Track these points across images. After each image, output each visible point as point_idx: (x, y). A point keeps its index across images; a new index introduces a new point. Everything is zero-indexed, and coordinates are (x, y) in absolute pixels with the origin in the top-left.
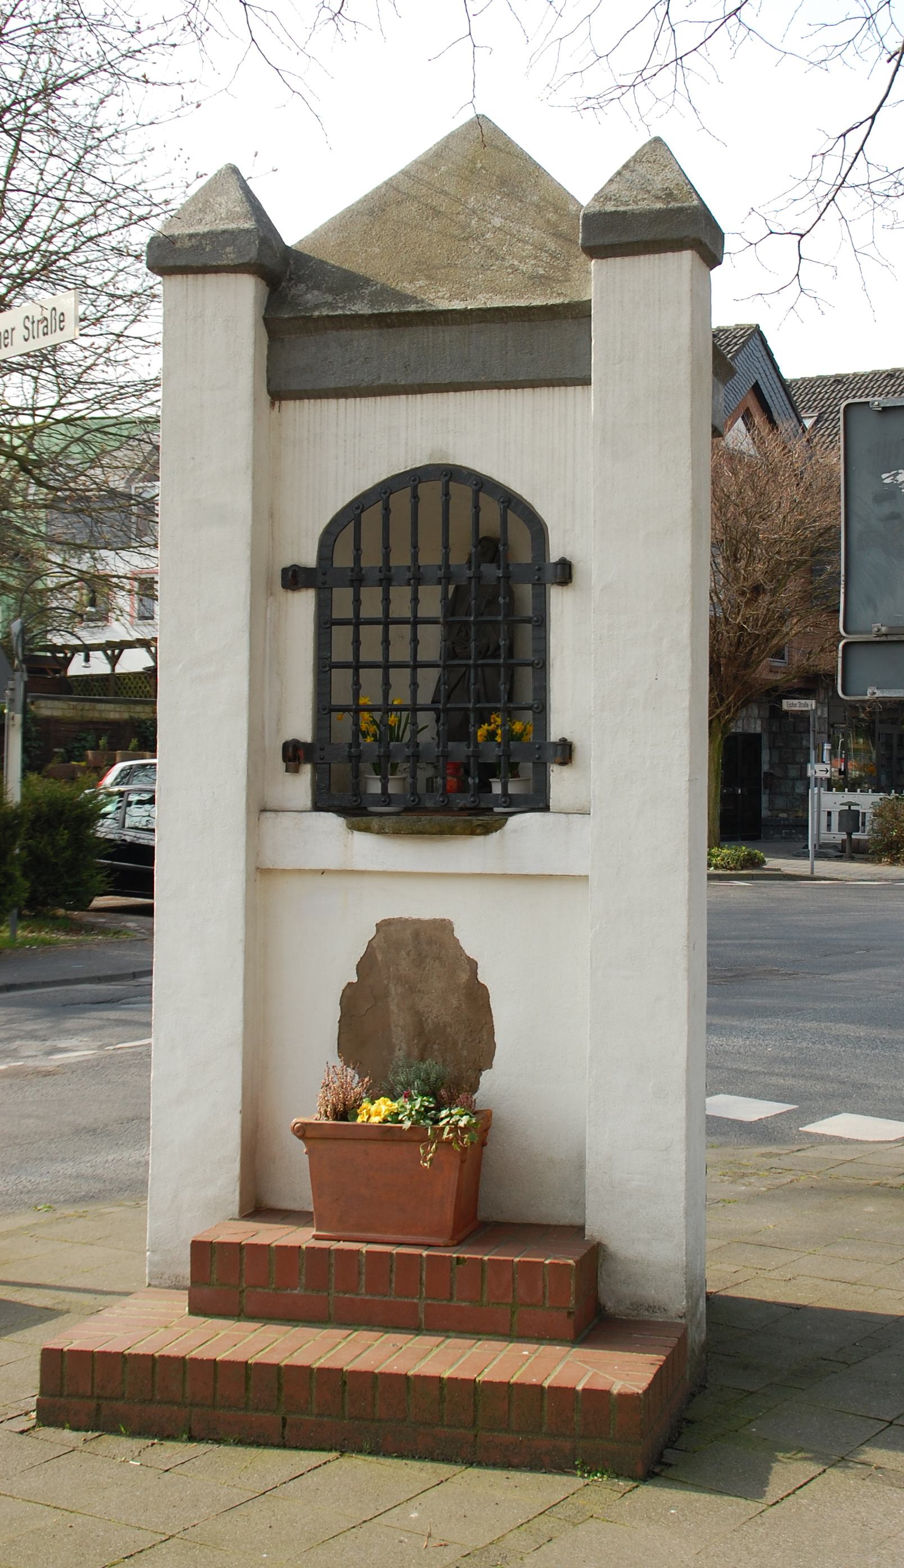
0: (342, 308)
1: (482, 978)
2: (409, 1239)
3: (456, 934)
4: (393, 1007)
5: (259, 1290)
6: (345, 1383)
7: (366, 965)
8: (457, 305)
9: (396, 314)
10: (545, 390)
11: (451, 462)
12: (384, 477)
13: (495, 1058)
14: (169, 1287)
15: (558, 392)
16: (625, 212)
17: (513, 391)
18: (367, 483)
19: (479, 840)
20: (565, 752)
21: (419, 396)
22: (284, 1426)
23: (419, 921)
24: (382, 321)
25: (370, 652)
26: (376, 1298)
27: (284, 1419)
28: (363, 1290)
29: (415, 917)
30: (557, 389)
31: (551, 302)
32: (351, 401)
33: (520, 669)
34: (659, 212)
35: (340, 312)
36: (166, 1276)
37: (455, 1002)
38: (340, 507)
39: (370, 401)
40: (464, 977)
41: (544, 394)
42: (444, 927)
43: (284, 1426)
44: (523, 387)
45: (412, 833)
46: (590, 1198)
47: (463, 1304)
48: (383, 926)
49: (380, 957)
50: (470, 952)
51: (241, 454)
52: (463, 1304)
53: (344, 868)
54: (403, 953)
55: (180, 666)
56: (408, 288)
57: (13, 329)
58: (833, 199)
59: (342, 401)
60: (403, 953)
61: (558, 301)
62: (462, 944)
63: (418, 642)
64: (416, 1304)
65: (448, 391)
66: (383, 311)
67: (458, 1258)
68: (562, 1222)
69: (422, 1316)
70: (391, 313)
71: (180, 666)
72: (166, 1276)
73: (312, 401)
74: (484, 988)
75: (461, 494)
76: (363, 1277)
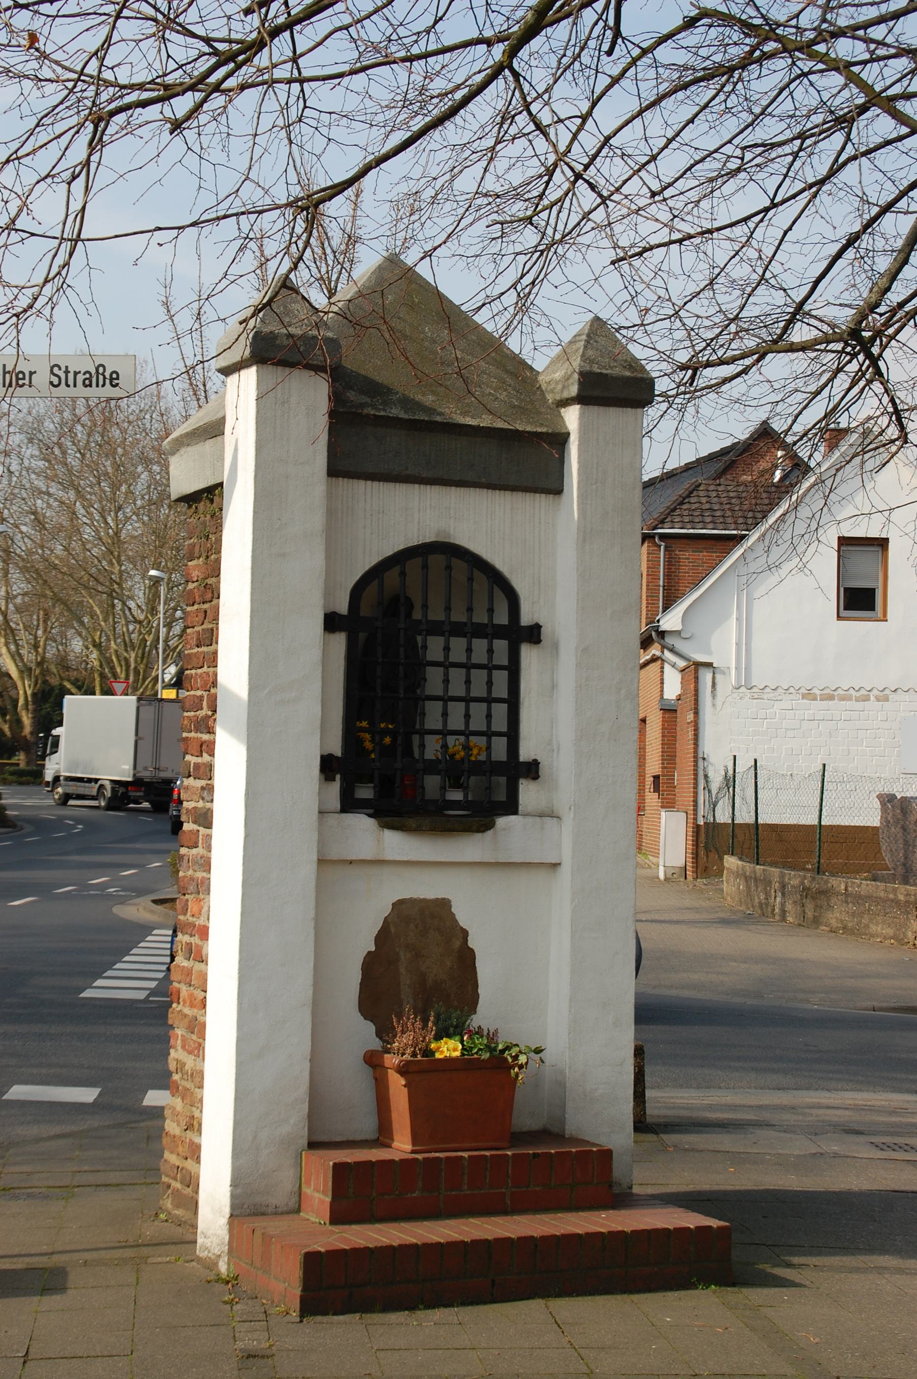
0: (384, 410)
1: (470, 944)
2: (480, 1144)
3: (453, 910)
4: (402, 970)
5: (386, 1197)
6: (536, 1246)
7: (382, 937)
8: (469, 421)
9: (427, 421)
10: (520, 494)
11: (452, 541)
12: (402, 547)
13: (479, 1006)
14: (249, 1215)
15: (529, 497)
16: (607, 375)
17: (497, 492)
18: (389, 551)
19: (479, 836)
20: (532, 770)
21: (429, 487)
22: (493, 1286)
23: (425, 900)
24: (414, 426)
25: (457, 688)
26: (475, 1192)
27: (493, 1281)
28: (466, 1187)
29: (422, 897)
30: (528, 494)
31: (539, 430)
32: (376, 484)
33: (428, 704)
34: (628, 378)
35: (382, 413)
36: (246, 1206)
37: (449, 964)
38: (367, 568)
39: (391, 486)
40: (457, 944)
41: (519, 497)
42: (444, 905)
43: (493, 1286)
44: (505, 490)
45: (445, 831)
46: (570, 1105)
47: (537, 1189)
48: (398, 905)
49: (393, 930)
50: (463, 922)
51: (317, 520)
52: (537, 1189)
53: (377, 858)
54: (412, 926)
55: (267, 691)
56: (428, 400)
57: (31, 373)
58: (847, 409)
59: (369, 483)
60: (412, 926)
61: (544, 430)
62: (457, 917)
63: (492, 684)
64: (505, 1193)
65: (451, 486)
66: (417, 417)
67: (534, 1154)
68: (524, 1129)
69: (509, 1202)
70: (423, 421)
71: (267, 691)
72: (246, 1206)
73: (346, 479)
74: (472, 950)
75: (460, 567)
76: (466, 1177)
